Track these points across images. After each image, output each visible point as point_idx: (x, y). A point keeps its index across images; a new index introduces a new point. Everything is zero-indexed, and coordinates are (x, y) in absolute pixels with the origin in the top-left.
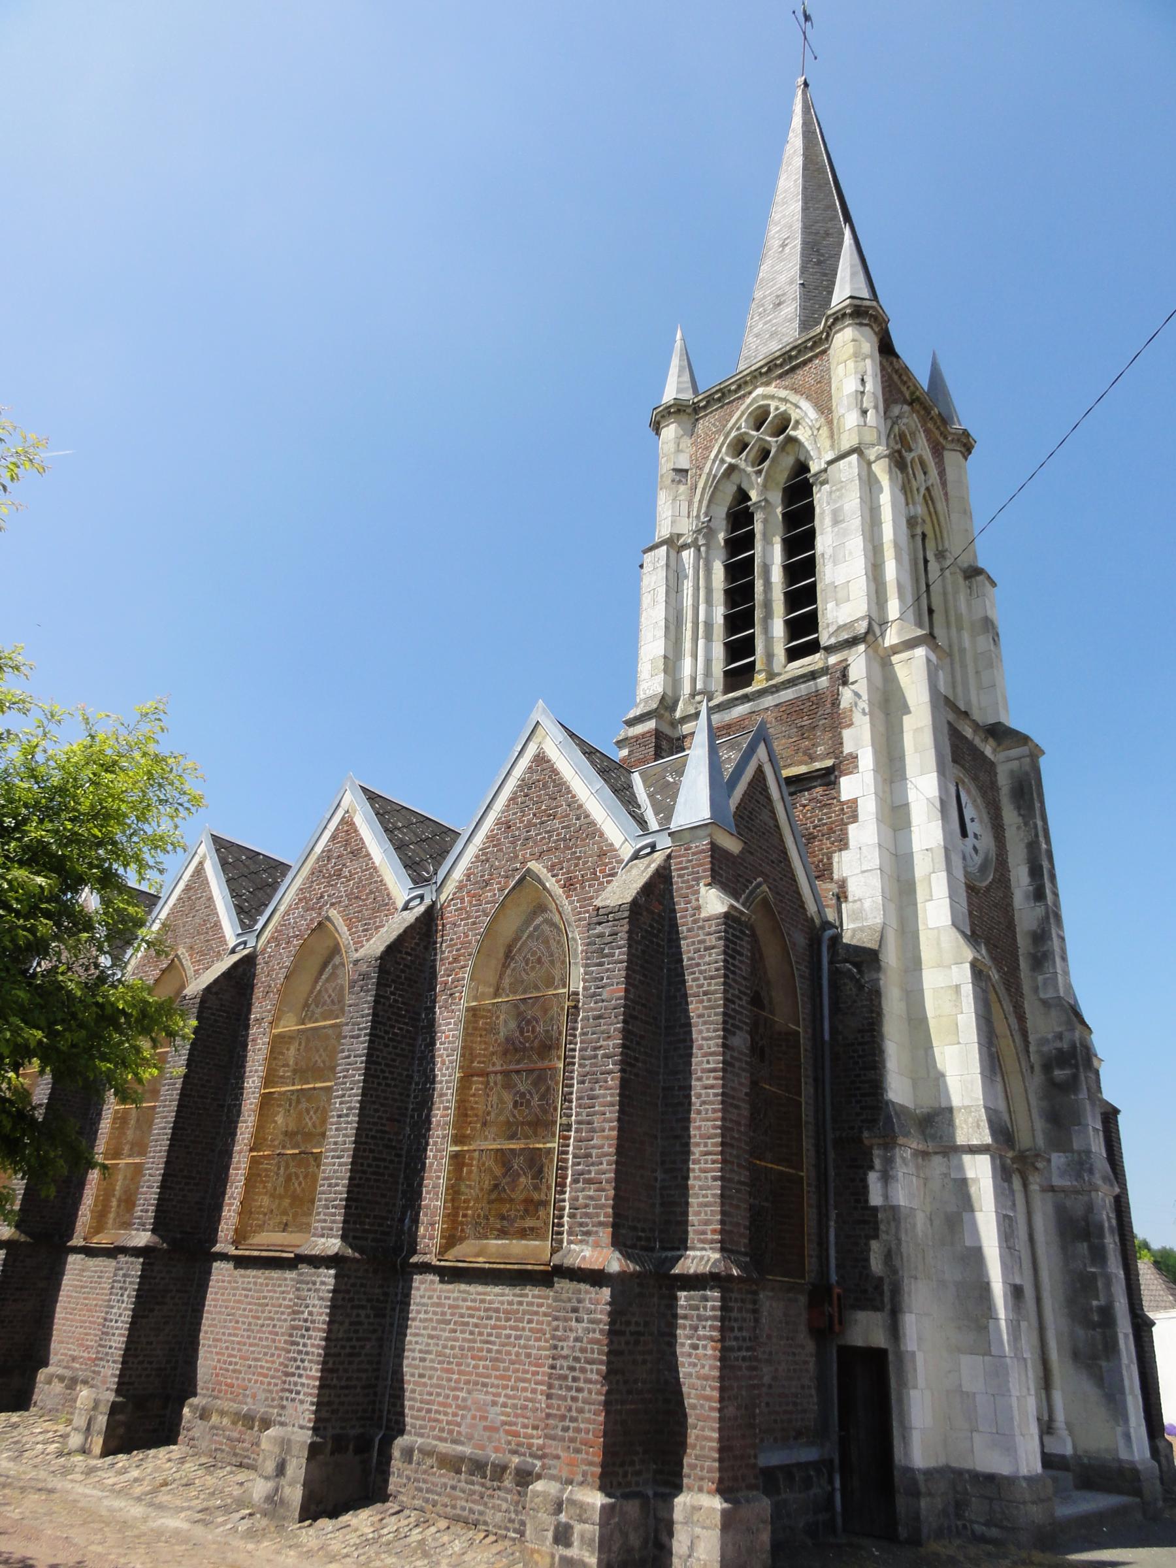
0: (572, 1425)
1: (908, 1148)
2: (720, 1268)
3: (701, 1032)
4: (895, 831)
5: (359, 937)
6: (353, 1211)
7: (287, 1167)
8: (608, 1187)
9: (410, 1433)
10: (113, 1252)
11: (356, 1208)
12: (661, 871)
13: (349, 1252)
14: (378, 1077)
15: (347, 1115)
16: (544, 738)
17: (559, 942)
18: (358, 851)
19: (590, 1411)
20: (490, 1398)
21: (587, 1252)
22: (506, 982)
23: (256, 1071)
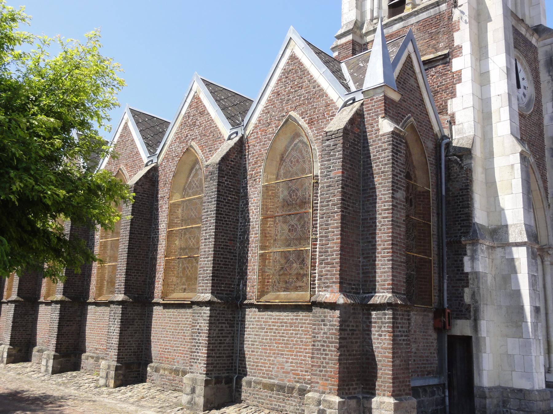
0: (324, 369)
1: (484, 245)
2: (392, 301)
3: (381, 191)
4: (481, 86)
5: (207, 155)
6: (215, 281)
7: (183, 264)
8: (337, 265)
9: (249, 375)
10: (107, 304)
11: (217, 280)
12: (358, 112)
13: (215, 299)
14: (222, 220)
15: (209, 239)
16: (294, 46)
17: (307, 151)
18: (203, 112)
19: (332, 364)
20: (285, 360)
21: (328, 295)
22: (282, 171)
23: (164, 221)
